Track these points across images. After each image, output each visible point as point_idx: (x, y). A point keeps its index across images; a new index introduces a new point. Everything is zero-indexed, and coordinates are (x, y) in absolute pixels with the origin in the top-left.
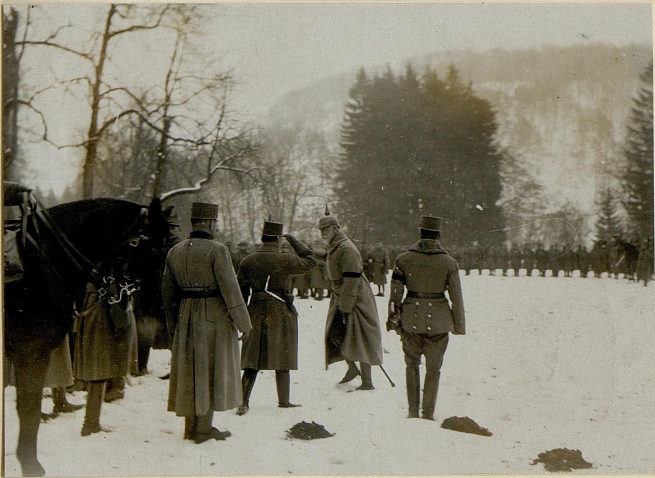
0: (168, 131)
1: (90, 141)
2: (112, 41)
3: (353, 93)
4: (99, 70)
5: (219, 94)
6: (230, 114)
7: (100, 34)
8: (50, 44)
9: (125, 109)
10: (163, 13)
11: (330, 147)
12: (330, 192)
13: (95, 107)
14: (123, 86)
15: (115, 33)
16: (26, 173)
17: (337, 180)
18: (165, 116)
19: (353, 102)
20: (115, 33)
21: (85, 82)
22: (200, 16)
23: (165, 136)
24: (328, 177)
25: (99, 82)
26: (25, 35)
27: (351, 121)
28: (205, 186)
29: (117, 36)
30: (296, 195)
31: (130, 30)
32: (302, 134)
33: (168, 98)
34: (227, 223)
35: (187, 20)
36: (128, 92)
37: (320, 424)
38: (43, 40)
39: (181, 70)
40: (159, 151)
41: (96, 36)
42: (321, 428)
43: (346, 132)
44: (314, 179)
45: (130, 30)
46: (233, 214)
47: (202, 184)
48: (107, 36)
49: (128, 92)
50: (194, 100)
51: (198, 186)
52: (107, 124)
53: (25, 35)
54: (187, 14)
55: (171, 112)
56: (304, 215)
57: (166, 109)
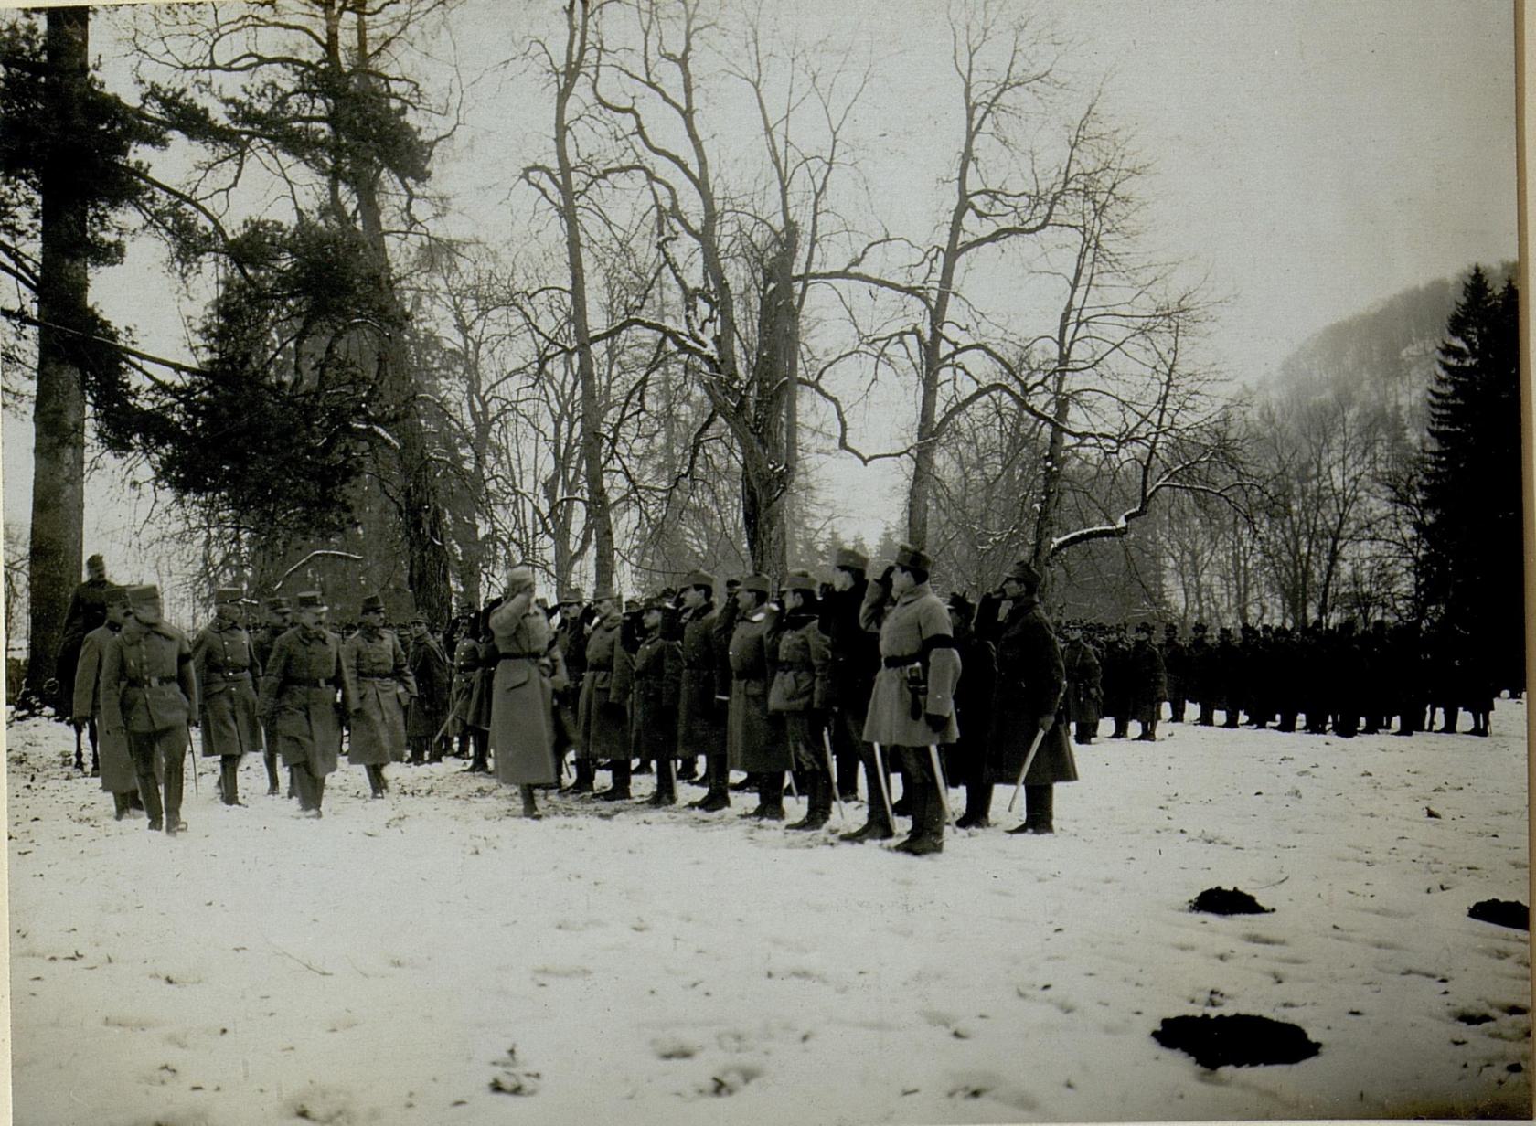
0: (1064, 419)
1: (920, 446)
2: (961, 261)
3: (1457, 326)
4: (937, 316)
5: (1163, 342)
6: (1184, 381)
7: (940, 249)
8: (824, 187)
9: (985, 382)
10: (1055, 199)
11: (1413, 437)
12: (1409, 531)
13: (930, 385)
14: (981, 341)
15: (969, 246)
16: (812, 510)
17: (1424, 506)
18: (1058, 392)
19: (1458, 343)
20: (969, 246)
21: (911, 340)
22: (1126, 200)
23: (1058, 430)
24: (1404, 501)
25: (937, 336)
26: (808, 264)
27: (1454, 383)
28: (1135, 523)
29: (972, 251)
30: (1336, 538)
31: (994, 238)
32: (1351, 414)
33: (1064, 358)
34: (1192, 596)
35: (1100, 211)
36: (990, 352)
37: (1248, 892)
38: (840, 268)
39: (1091, 302)
40: (1047, 459)
41: (932, 254)
42: (1251, 899)
43: (1441, 407)
44: (1378, 505)
45: (994, 238)
46: (1204, 579)
47: (1127, 519)
48: (953, 253)
49: (990, 352)
50: (1115, 359)
51: (1121, 523)
52: (949, 415)
53: (808, 264)
54: (1101, 198)
55: (1072, 383)
56: (1356, 581)
57: (1060, 381)
